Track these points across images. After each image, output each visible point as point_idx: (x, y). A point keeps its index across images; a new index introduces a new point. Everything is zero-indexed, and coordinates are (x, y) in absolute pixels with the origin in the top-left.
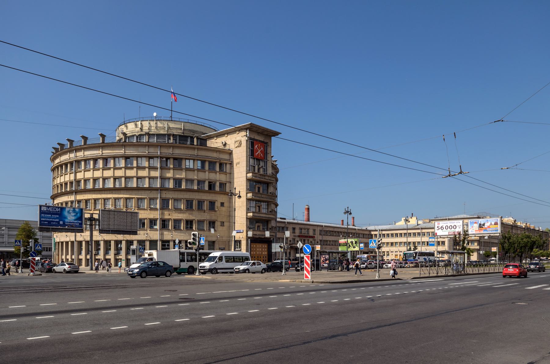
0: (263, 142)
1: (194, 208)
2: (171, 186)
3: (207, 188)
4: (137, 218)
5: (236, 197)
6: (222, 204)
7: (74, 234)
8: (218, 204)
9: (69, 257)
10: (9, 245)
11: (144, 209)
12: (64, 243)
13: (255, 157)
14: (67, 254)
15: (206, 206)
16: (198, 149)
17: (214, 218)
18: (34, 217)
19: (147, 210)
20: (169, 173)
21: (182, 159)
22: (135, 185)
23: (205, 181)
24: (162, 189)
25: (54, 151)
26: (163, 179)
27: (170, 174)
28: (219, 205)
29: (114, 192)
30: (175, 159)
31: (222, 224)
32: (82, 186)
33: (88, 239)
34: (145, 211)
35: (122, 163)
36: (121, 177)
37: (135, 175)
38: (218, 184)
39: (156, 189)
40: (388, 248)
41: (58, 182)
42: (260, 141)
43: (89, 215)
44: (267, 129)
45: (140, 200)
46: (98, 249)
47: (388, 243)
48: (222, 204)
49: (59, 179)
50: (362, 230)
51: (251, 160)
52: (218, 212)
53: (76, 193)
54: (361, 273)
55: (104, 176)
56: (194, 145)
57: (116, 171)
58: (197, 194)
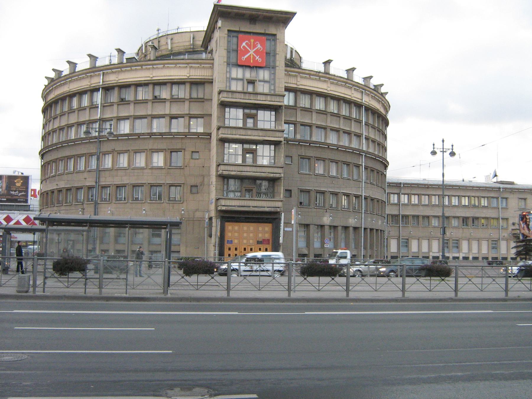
18: (286, 43)
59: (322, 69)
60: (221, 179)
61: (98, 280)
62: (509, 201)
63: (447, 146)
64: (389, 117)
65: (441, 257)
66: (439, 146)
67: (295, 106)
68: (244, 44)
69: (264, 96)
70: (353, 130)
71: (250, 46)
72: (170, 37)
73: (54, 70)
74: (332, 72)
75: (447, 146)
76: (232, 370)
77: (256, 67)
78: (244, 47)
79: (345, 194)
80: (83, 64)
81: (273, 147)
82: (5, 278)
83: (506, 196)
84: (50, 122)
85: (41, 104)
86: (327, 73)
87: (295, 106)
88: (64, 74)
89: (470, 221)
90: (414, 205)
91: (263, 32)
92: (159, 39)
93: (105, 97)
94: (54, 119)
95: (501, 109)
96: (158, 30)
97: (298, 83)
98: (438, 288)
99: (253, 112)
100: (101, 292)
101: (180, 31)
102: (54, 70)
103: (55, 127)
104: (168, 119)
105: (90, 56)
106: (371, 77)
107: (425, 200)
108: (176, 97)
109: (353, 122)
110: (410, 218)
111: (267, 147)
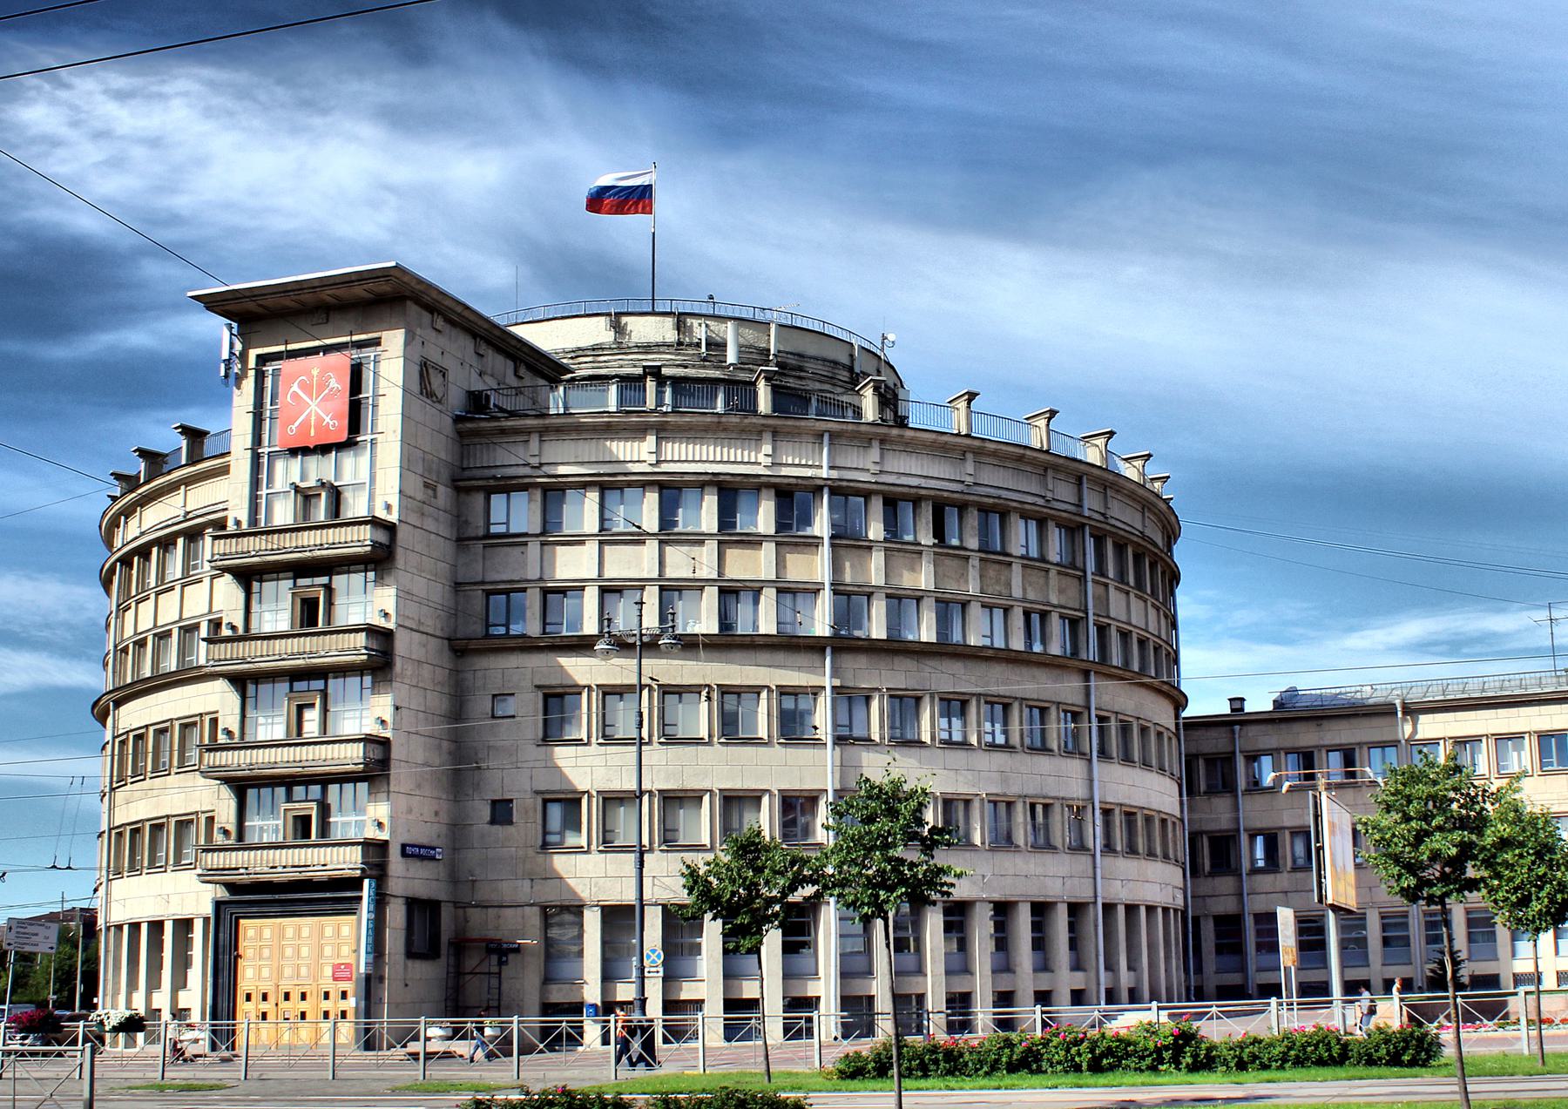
2: (706, 623)
9: (162, 1000)
10: (1335, 892)
11: (697, 742)
12: (144, 928)
14: (154, 984)
15: (762, 720)
16: (776, 434)
19: (710, 743)
20: (913, 569)
22: (767, 626)
24: (843, 644)
26: (729, 593)
27: (875, 570)
29: (780, 657)
30: (985, 510)
34: (761, 749)
36: (640, 585)
39: (815, 646)
41: (145, 623)
46: (182, 962)
49: (146, 609)
55: (669, 573)
56: (755, 412)
57: (732, 554)
58: (883, 663)
68: (295, 388)
78: (295, 395)
108: (502, 529)
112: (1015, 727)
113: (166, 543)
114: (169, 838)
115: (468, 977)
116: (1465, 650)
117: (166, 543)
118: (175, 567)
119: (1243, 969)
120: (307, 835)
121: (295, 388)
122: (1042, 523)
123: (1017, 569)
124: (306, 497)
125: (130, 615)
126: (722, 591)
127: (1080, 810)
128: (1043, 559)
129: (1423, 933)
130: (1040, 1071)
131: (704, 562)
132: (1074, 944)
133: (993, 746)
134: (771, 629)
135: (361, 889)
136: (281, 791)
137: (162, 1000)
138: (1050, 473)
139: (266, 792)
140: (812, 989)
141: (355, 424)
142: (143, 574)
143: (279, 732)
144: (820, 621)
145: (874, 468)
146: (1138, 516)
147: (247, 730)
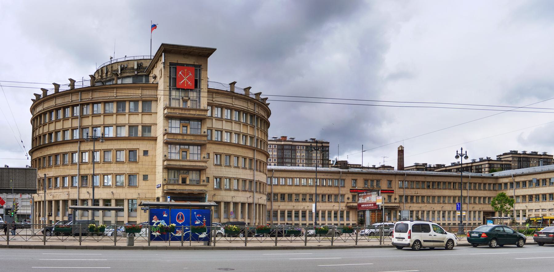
0: (194, 65)
1: (59, 185)
2: (77, 136)
3: (180, 182)
4: (36, 176)
5: (463, 157)
6: (146, 153)
7: (119, 136)
8: (140, 153)
12: (53, 202)
13: (177, 87)
14: (57, 215)
17: (135, 171)
18: (495, 158)
21: (125, 101)
23: (138, 126)
25: (34, 98)
28: (141, 153)
31: (145, 178)
32: (60, 138)
33: (43, 199)
35: (113, 108)
37: (127, 122)
38: (140, 128)
40: (524, 205)
41: (37, 134)
42: (187, 65)
43: (351, 214)
44: (191, 47)
45: (132, 177)
47: (524, 196)
48: (146, 153)
49: (41, 129)
50: (374, 167)
51: (174, 93)
52: (140, 163)
53: (81, 142)
54: (401, 152)
55: (118, 123)
59: (229, 90)
60: (165, 171)
61: (219, 140)
62: (346, 182)
63: (464, 153)
64: (270, 119)
65: (314, 224)
66: (460, 152)
67: (212, 116)
68: (180, 73)
69: (423, 177)
70: (249, 133)
71: (184, 75)
72: (120, 64)
73: (35, 94)
74: (236, 91)
75: (464, 153)
76: (79, 193)
77: (188, 89)
79: (235, 156)
80: (51, 92)
81: (199, 147)
82: (552, 217)
83: (344, 178)
84: (36, 129)
85: (31, 116)
86: (232, 92)
87: (212, 116)
88: (49, 93)
89: (521, 184)
90: (282, 185)
91: (77, 244)
92: (112, 65)
93: (82, 111)
94: (43, 126)
95: (525, 93)
96: (111, 58)
97: (214, 100)
98: (30, 240)
99: (187, 147)
100: (306, 245)
101: (127, 59)
102: (35, 94)
103: (50, 130)
104: (115, 127)
105: (54, 84)
106: (250, 88)
107: (303, 182)
109: (233, 123)
110: (447, 183)
111: (196, 147)
112: (318, 155)
113: (45, 114)
114: (333, 197)
115: (409, 162)
116: (404, 248)
117: (45, 114)
118: (61, 116)
119: (292, 220)
120: (284, 199)
121: (180, 73)
122: (231, 133)
123: (242, 125)
124: (401, 196)
125: (37, 131)
126: (129, 126)
127: (270, 211)
128: (231, 119)
129: (286, 203)
130: (157, 84)
131: (76, 123)
132: (242, 212)
133: (329, 186)
134: (78, 137)
135: (123, 205)
136: (77, 86)
137: (313, 222)
138: (214, 95)
139: (173, 171)
140: (432, 232)
141: (196, 86)
142: (41, 121)
143: (125, 244)
144: (466, 222)
145: (115, 96)
146: (253, 106)
147: (106, 158)
